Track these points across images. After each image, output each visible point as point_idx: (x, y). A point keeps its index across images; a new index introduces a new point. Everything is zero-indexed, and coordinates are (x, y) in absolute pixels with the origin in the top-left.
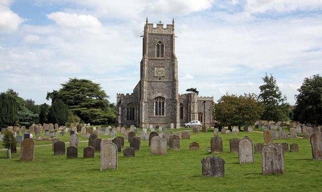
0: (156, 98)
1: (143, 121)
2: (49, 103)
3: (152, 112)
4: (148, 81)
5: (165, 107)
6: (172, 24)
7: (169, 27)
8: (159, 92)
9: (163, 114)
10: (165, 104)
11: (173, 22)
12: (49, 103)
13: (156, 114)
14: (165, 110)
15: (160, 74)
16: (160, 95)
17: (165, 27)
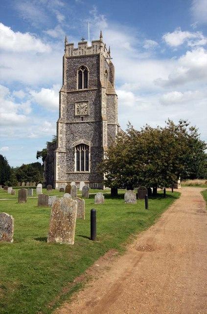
0: (76, 147)
1: (57, 179)
2: (40, 160)
3: (72, 167)
4: (67, 124)
5: (90, 159)
6: (99, 39)
7: (95, 44)
8: (81, 137)
9: (87, 169)
10: (90, 155)
11: (101, 37)
12: (40, 160)
13: (78, 169)
14: (90, 162)
15: (83, 112)
16: (82, 141)
17: (89, 45)
